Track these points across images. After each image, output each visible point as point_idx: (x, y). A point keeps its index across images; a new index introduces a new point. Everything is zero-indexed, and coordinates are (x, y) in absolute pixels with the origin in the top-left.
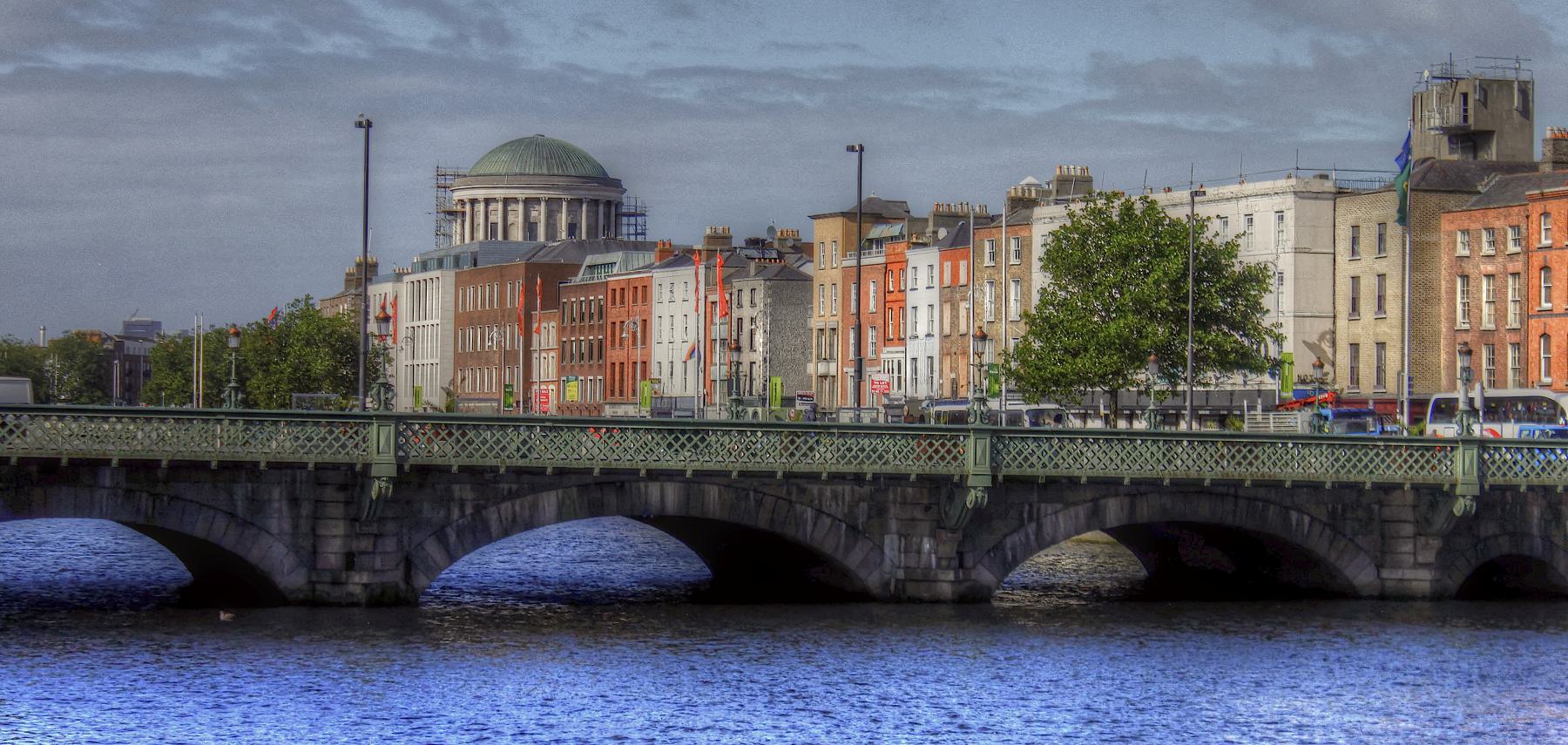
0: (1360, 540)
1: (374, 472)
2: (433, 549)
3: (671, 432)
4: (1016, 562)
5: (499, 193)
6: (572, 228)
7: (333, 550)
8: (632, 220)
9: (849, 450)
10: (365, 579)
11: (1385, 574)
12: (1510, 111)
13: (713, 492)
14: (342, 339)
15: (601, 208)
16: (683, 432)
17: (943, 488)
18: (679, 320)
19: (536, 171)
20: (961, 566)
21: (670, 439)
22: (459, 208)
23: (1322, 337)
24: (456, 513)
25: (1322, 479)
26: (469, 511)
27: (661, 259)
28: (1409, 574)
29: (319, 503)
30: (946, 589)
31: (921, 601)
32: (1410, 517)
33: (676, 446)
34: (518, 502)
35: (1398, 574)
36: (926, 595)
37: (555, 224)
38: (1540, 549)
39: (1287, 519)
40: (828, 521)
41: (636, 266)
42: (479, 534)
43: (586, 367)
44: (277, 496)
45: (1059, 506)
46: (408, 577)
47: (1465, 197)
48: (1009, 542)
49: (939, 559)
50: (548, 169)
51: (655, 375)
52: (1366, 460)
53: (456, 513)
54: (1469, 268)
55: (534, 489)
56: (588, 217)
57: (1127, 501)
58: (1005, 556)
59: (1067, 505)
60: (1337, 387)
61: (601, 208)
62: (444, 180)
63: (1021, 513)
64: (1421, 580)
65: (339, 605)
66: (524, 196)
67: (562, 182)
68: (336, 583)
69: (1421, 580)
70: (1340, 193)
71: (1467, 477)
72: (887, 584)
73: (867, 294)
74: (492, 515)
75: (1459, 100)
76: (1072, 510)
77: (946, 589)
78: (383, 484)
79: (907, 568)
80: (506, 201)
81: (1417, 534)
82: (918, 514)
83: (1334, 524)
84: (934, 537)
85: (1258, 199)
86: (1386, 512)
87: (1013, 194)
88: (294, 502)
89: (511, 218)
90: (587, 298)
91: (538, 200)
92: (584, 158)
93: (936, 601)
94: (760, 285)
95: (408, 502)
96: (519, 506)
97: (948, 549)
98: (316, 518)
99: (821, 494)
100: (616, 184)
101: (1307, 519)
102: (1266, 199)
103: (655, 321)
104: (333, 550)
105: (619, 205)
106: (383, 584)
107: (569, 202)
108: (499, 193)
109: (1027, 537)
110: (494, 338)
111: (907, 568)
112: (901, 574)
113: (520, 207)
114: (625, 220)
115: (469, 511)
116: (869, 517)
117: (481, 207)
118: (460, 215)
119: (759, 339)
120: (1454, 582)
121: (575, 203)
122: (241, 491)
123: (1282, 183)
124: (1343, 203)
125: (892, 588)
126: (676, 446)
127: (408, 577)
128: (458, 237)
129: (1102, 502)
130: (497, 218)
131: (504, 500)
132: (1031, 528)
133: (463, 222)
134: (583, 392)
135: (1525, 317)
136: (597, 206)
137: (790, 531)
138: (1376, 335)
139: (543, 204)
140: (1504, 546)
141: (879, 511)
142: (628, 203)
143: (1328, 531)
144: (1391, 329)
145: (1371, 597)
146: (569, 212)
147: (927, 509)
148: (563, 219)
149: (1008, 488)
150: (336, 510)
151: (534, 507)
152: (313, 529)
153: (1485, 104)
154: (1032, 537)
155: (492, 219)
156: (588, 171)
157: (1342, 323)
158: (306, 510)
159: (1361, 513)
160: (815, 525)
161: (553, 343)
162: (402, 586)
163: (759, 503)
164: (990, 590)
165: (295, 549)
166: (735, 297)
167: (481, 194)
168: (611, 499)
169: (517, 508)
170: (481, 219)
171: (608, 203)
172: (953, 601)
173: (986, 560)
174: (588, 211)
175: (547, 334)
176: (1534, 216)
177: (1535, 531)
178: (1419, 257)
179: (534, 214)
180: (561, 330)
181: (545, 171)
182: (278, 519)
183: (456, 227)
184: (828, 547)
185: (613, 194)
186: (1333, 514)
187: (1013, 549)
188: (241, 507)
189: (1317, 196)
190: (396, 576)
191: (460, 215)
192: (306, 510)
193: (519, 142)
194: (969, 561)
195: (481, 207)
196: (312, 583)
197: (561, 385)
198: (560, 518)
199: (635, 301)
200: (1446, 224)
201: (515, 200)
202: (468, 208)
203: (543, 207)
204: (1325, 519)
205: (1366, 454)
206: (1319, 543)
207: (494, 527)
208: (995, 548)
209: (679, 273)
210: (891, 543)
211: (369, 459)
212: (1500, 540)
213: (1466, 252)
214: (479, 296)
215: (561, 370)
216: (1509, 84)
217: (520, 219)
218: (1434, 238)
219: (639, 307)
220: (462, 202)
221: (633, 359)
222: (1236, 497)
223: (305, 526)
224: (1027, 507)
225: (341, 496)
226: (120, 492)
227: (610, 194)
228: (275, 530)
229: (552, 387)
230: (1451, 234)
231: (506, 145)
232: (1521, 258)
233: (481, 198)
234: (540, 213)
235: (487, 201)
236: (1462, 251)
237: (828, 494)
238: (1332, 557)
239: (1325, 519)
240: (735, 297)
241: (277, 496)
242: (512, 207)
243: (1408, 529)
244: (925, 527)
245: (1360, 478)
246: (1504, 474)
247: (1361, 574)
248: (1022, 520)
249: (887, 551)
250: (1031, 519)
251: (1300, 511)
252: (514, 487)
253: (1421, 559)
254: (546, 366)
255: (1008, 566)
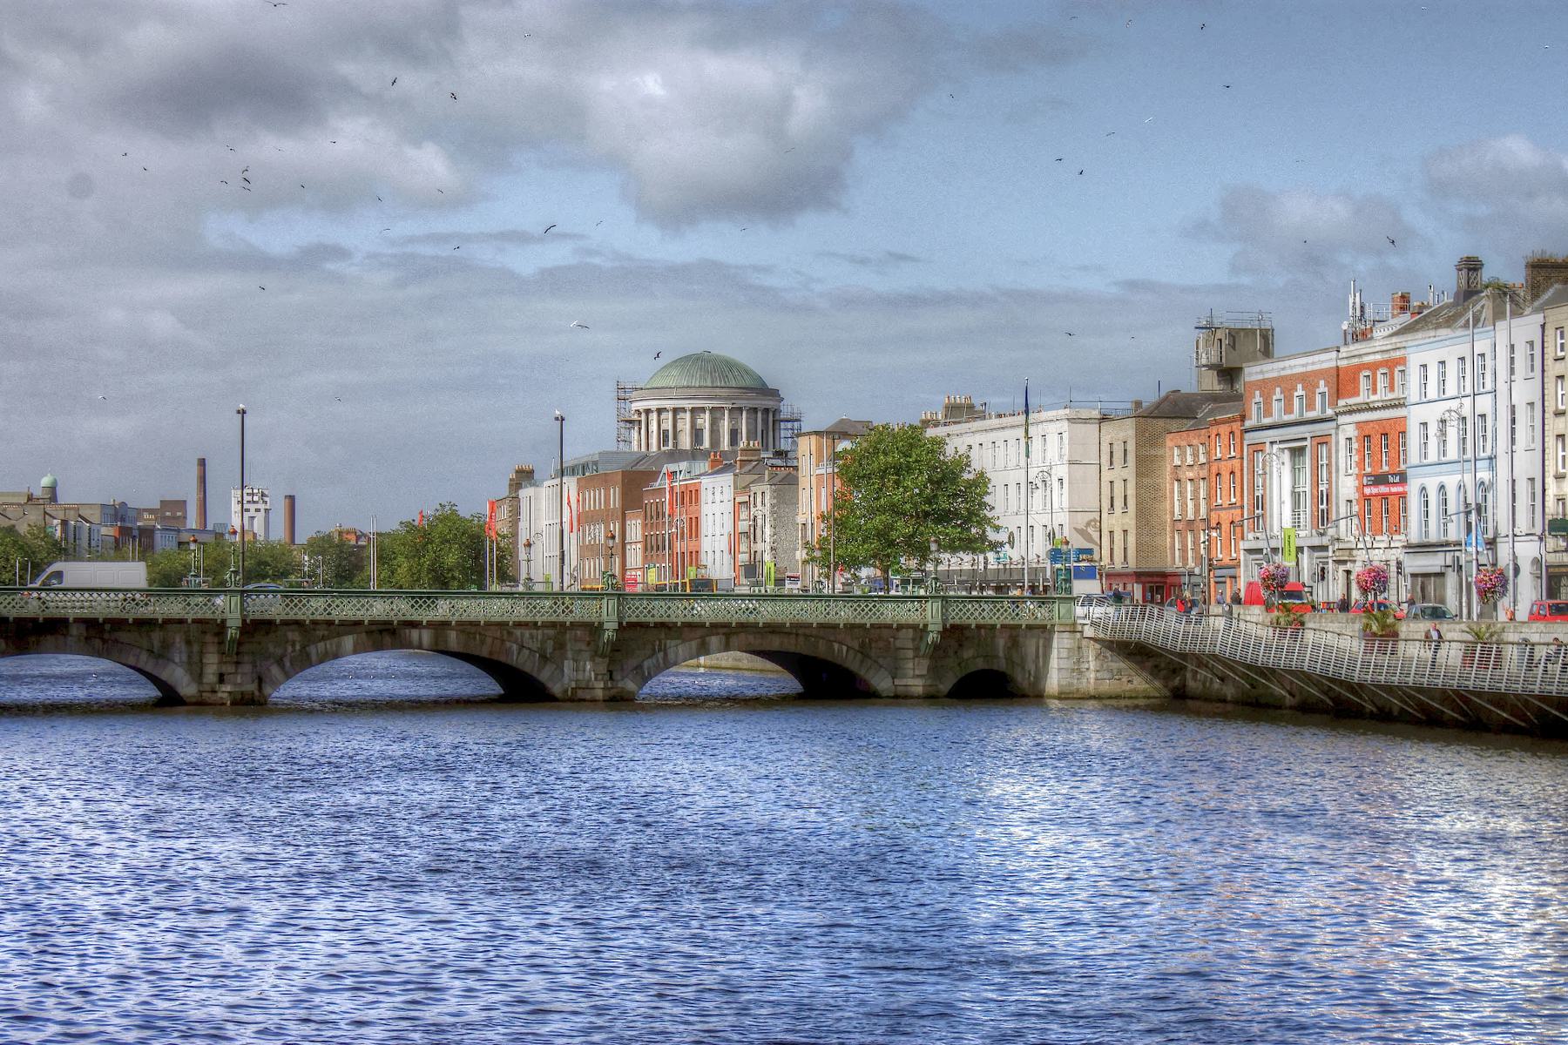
0: (881, 661)
1: (229, 624)
2: (275, 671)
3: (413, 598)
4: (650, 677)
5: (669, 404)
6: (734, 435)
7: (210, 675)
8: (789, 425)
9: (535, 608)
10: (229, 688)
11: (897, 682)
12: (1255, 352)
13: (453, 635)
14: (472, 537)
15: (759, 415)
16: (421, 598)
17: (594, 629)
18: (718, 515)
19: (702, 384)
20: (611, 678)
21: (413, 602)
22: (636, 417)
23: (1088, 524)
24: (290, 649)
25: (837, 622)
26: (298, 647)
27: (712, 467)
28: (910, 682)
29: (203, 644)
30: (599, 694)
31: (584, 700)
32: (911, 646)
33: (416, 606)
34: (328, 642)
35: (904, 682)
36: (588, 697)
37: (719, 431)
38: (1004, 666)
39: (832, 648)
40: (527, 652)
41: (698, 473)
42: (304, 661)
43: (649, 557)
44: (179, 640)
45: (679, 641)
46: (260, 688)
47: (1185, 421)
48: (646, 664)
49: (596, 675)
50: (712, 382)
51: (704, 563)
52: (866, 610)
53: (290, 649)
54: (1181, 476)
55: (339, 635)
56: (747, 423)
57: (723, 637)
58: (644, 672)
59: (684, 641)
60: (1102, 564)
61: (759, 415)
62: (623, 394)
63: (654, 646)
64: (917, 686)
65: (215, 705)
66: (691, 406)
67: (724, 392)
68: (214, 692)
69: (917, 686)
70: (1104, 419)
71: (1063, 621)
72: (566, 691)
73: (538, 510)
74: (312, 650)
75: (1217, 343)
76: (687, 644)
77: (599, 694)
78: (234, 631)
79: (577, 681)
80: (676, 411)
81: (916, 656)
82: (584, 647)
83: (864, 651)
84: (594, 661)
85: (1048, 423)
86: (899, 644)
87: (924, 418)
88: (188, 643)
89: (680, 426)
90: (655, 500)
91: (703, 410)
92: (747, 372)
93: (594, 701)
94: (767, 489)
95: (260, 643)
96: (330, 645)
97: (603, 669)
98: (201, 653)
99: (522, 635)
100: (774, 394)
101: (845, 648)
102: (1052, 423)
103: (703, 520)
104: (210, 675)
105: (776, 411)
106: (242, 693)
107: (731, 410)
108: (688, 404)
109: (658, 661)
110: (599, 533)
111: (577, 681)
112: (573, 685)
113: (688, 416)
114: (783, 425)
115: (298, 647)
116: (554, 650)
117: (654, 416)
118: (637, 423)
119: (768, 531)
120: (945, 687)
121: (736, 411)
122: (156, 637)
123: (1062, 412)
124: (1105, 426)
125: (569, 693)
126: (416, 606)
127: (260, 688)
128: (636, 443)
129: (707, 639)
130: (668, 425)
131: (320, 641)
132: (661, 655)
133: (640, 429)
134: (659, 576)
135: (1210, 510)
136: (756, 413)
137: (503, 659)
138: (1123, 524)
139: (707, 412)
140: (980, 664)
141: (560, 646)
142: (785, 411)
143: (859, 655)
144: (1130, 521)
145: (888, 697)
146: (731, 419)
147: (589, 644)
148: (725, 426)
149: (625, 628)
150: (212, 648)
151: (339, 646)
152: (201, 661)
153: (1234, 348)
154: (661, 661)
155: (664, 427)
156: (748, 382)
157: (1105, 515)
158: (196, 648)
159: (881, 644)
160: (519, 654)
161: (640, 538)
162: (257, 693)
163: (483, 642)
164: (633, 693)
165: (190, 671)
166: (752, 499)
167: (653, 405)
168: (387, 639)
169: (328, 646)
170: (654, 427)
171: (766, 411)
172: (604, 701)
173: (630, 676)
174: (747, 418)
175: (635, 529)
176: (1213, 436)
177: (1001, 654)
178: (1146, 465)
179: (699, 421)
180: (645, 526)
181: (709, 384)
182: (179, 654)
183: (635, 434)
184: (527, 668)
185: (771, 403)
186: (862, 645)
187: (649, 668)
188: (157, 644)
189: (1086, 421)
190: (251, 687)
191: (637, 423)
192: (196, 648)
193: (687, 358)
194: (617, 676)
195: (654, 416)
196: (201, 692)
197: (645, 570)
198: (355, 652)
199: (691, 502)
200: (1169, 441)
201: (683, 410)
202: (643, 417)
203: (707, 415)
204: (857, 648)
205: (867, 606)
206: (853, 663)
207: (314, 658)
208: (636, 668)
209: (718, 479)
210: (568, 666)
211: (225, 616)
212: (977, 660)
213: (1179, 463)
214: (596, 499)
215: (645, 558)
216: (1253, 331)
217: (688, 426)
218: (1160, 452)
219: (693, 507)
220: (639, 413)
221: (690, 549)
222: (797, 635)
223: (196, 658)
224: (657, 643)
225: (216, 640)
226: (82, 638)
227: (769, 403)
228: (177, 660)
229: (639, 573)
230: (1171, 449)
231: (675, 361)
232: (1206, 466)
233: (654, 408)
234: (705, 421)
235: (660, 411)
236: (1177, 462)
237: (527, 635)
238: (862, 673)
239: (857, 648)
240: (752, 499)
241: (179, 640)
242: (663, 416)
243: (910, 654)
244: (587, 655)
245: (863, 621)
246: (961, 618)
247: (882, 683)
248: (654, 650)
249: (566, 670)
250: (660, 650)
251: (841, 643)
252: (326, 633)
253: (917, 672)
254: (635, 556)
255: (645, 680)
